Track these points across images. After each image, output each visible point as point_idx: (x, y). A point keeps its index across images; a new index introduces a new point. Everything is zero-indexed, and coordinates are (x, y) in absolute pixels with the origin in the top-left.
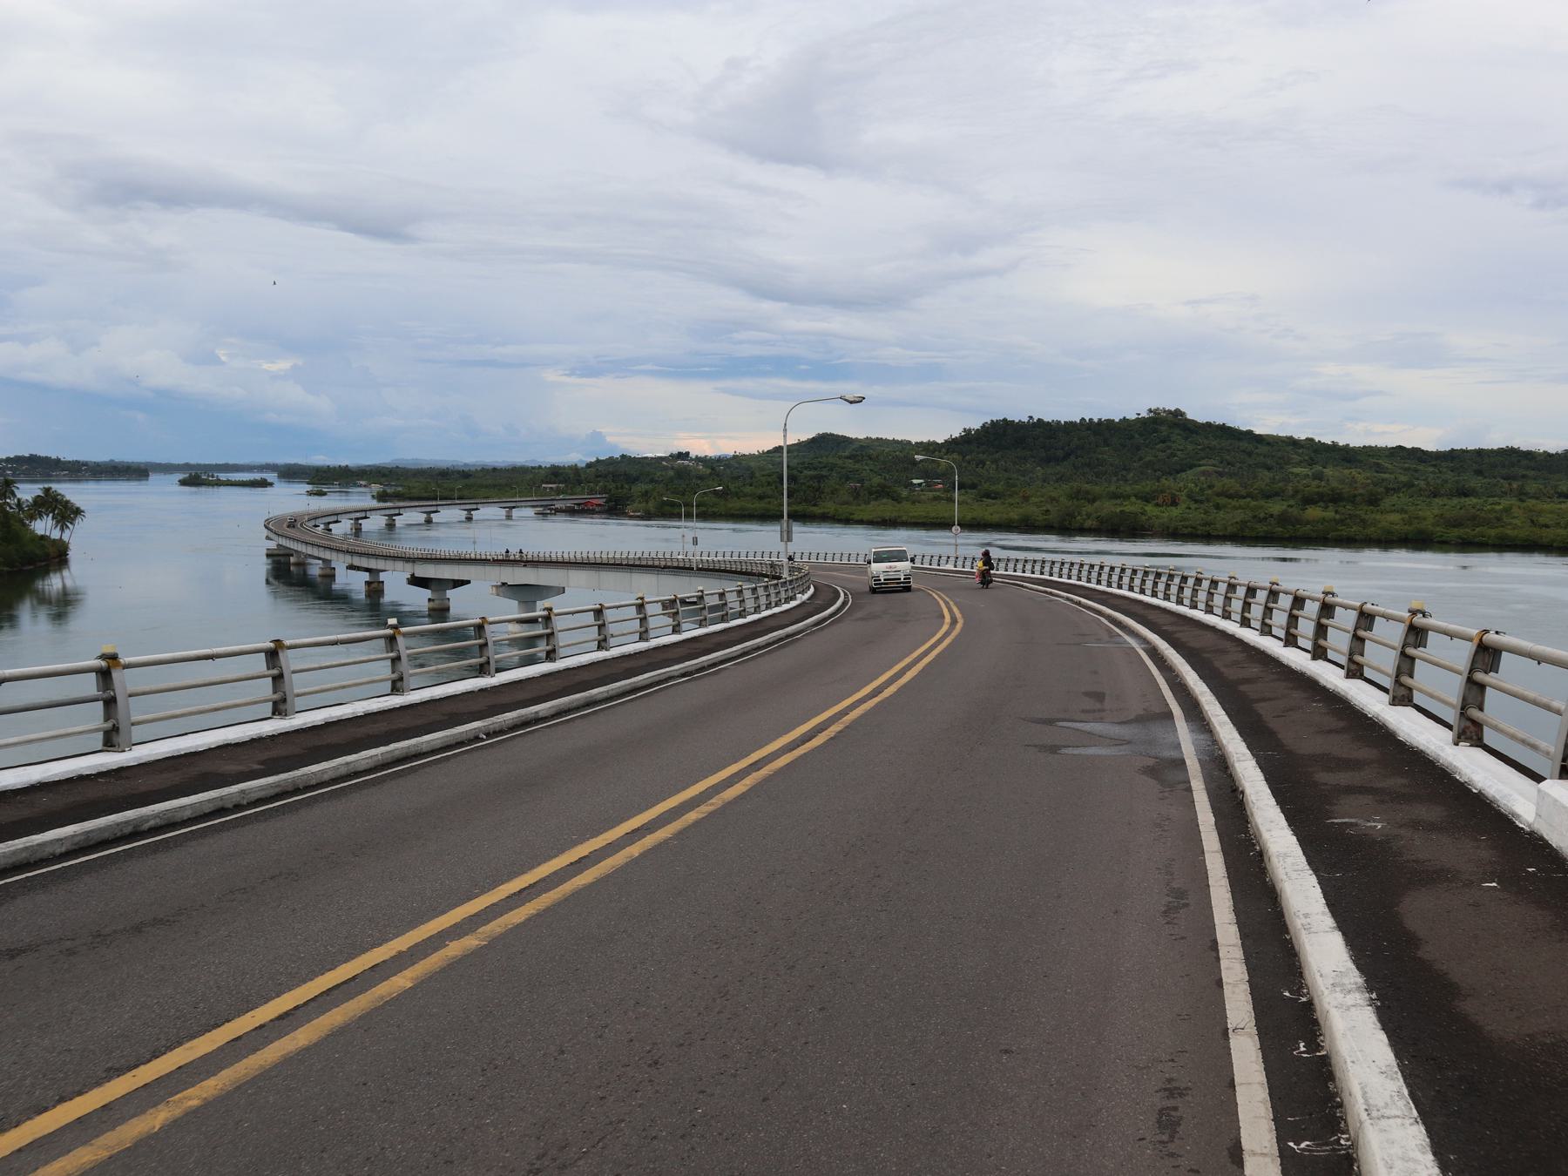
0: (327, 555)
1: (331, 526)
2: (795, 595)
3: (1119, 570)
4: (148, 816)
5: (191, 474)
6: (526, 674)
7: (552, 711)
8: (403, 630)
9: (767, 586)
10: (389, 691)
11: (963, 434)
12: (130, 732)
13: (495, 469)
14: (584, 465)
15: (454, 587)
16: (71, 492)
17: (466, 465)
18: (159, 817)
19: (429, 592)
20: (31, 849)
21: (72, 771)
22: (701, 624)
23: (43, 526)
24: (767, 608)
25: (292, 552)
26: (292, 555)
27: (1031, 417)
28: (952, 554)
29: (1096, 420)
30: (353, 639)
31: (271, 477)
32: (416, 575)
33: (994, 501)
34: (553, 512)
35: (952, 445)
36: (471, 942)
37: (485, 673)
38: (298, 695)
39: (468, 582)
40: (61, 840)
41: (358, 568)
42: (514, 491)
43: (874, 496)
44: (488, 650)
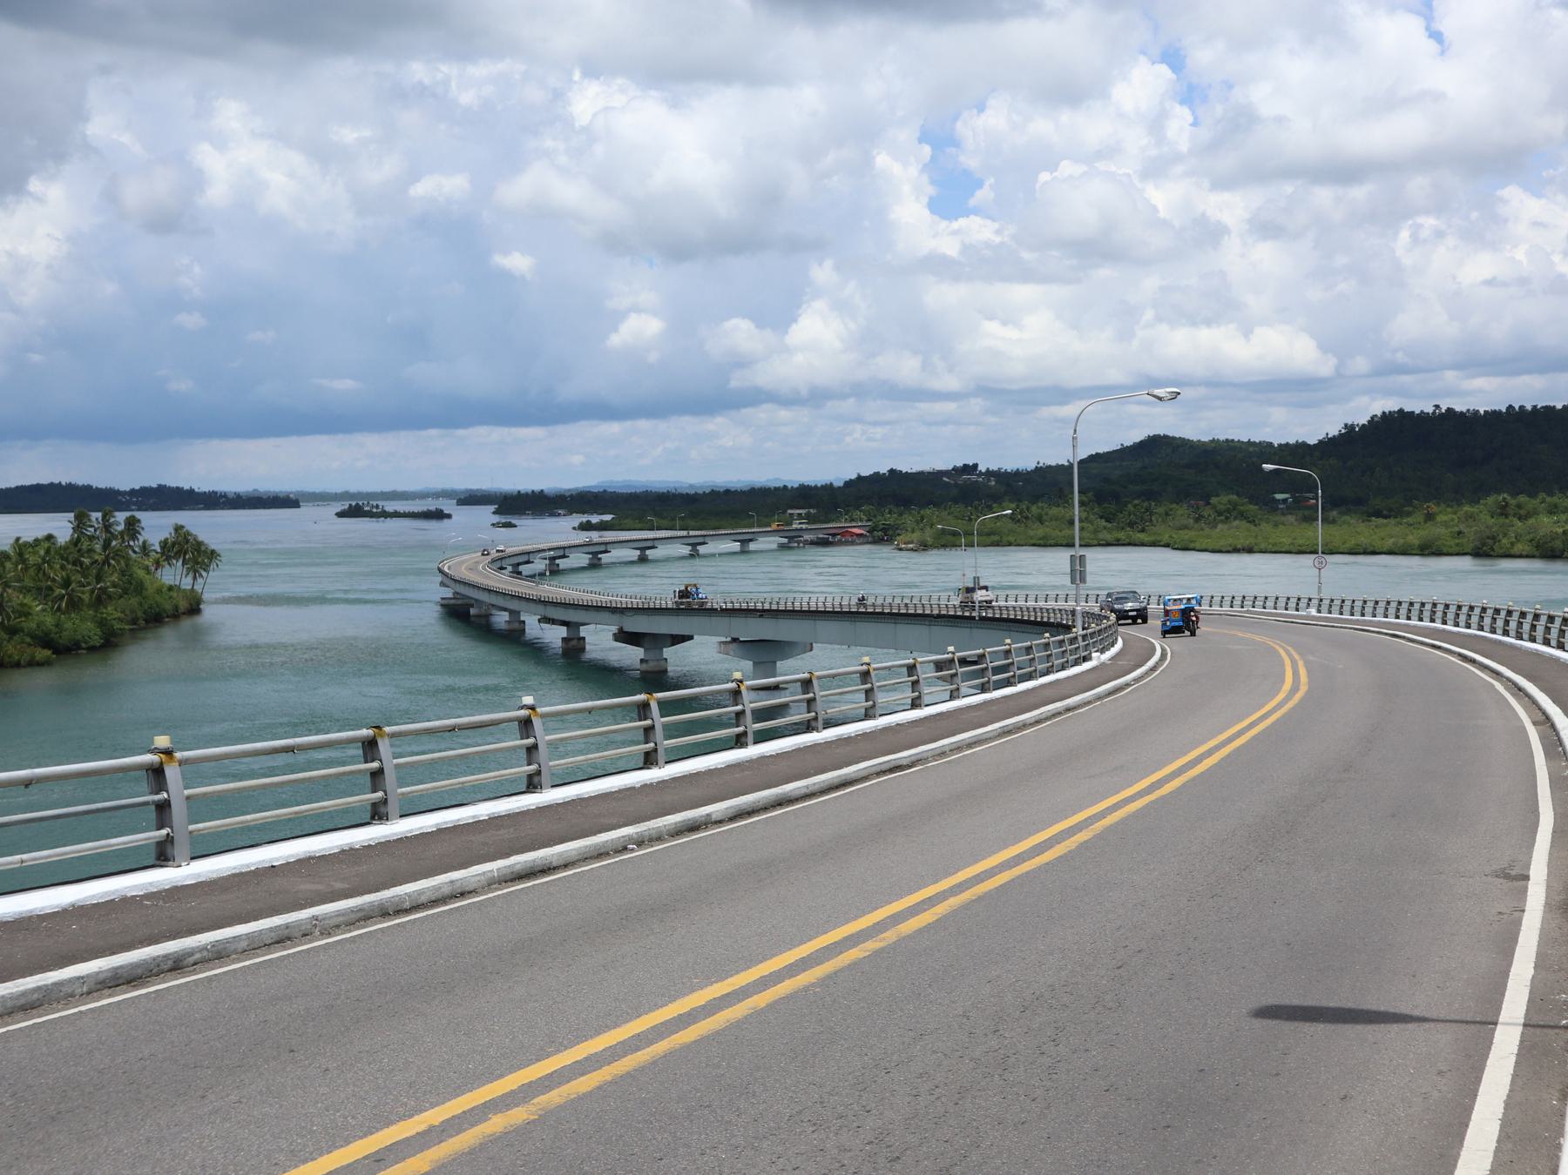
0: (514, 605)
1: (521, 568)
2: (1090, 654)
4: (192, 948)
5: (350, 505)
6: (706, 765)
7: (730, 813)
8: (387, 729)
9: (1031, 647)
11: (1343, 431)
13: (727, 492)
14: (841, 484)
15: (673, 645)
16: (203, 525)
17: (691, 486)
18: (208, 950)
19: (642, 650)
20: (45, 989)
21: (113, 892)
22: (983, 689)
23: (173, 575)
25: (473, 602)
26: (472, 606)
27: (1437, 407)
28: (1315, 595)
29: (1529, 408)
31: (447, 506)
32: (626, 629)
33: (1385, 521)
34: (801, 545)
35: (1328, 446)
36: (519, 1115)
37: (652, 764)
39: (690, 638)
40: (83, 978)
41: (553, 621)
42: (752, 520)
43: (1223, 518)
44: (654, 734)
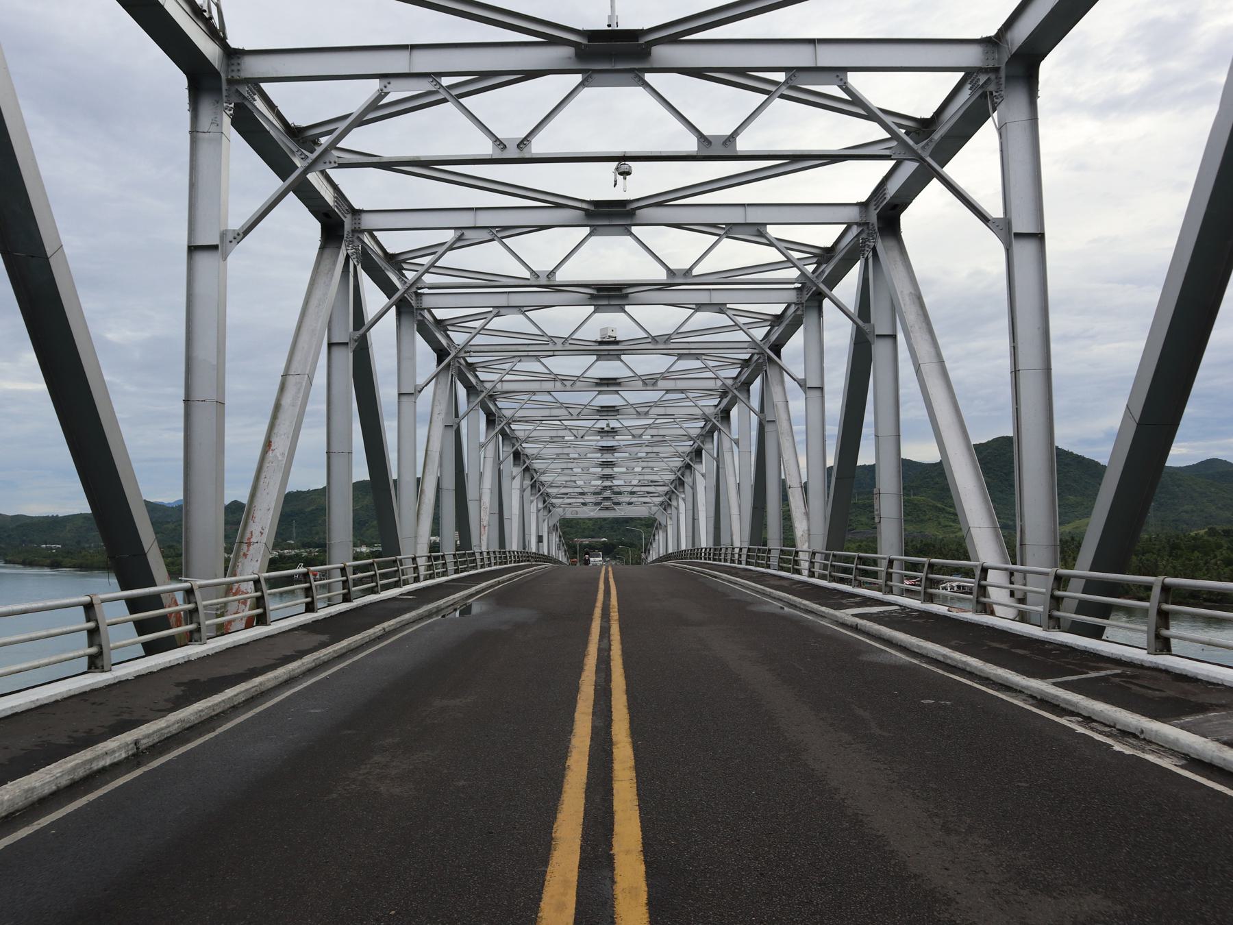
3: (746, 550)
10: (304, 611)
12: (110, 653)
24: (481, 568)
30: (117, 597)
38: (271, 611)
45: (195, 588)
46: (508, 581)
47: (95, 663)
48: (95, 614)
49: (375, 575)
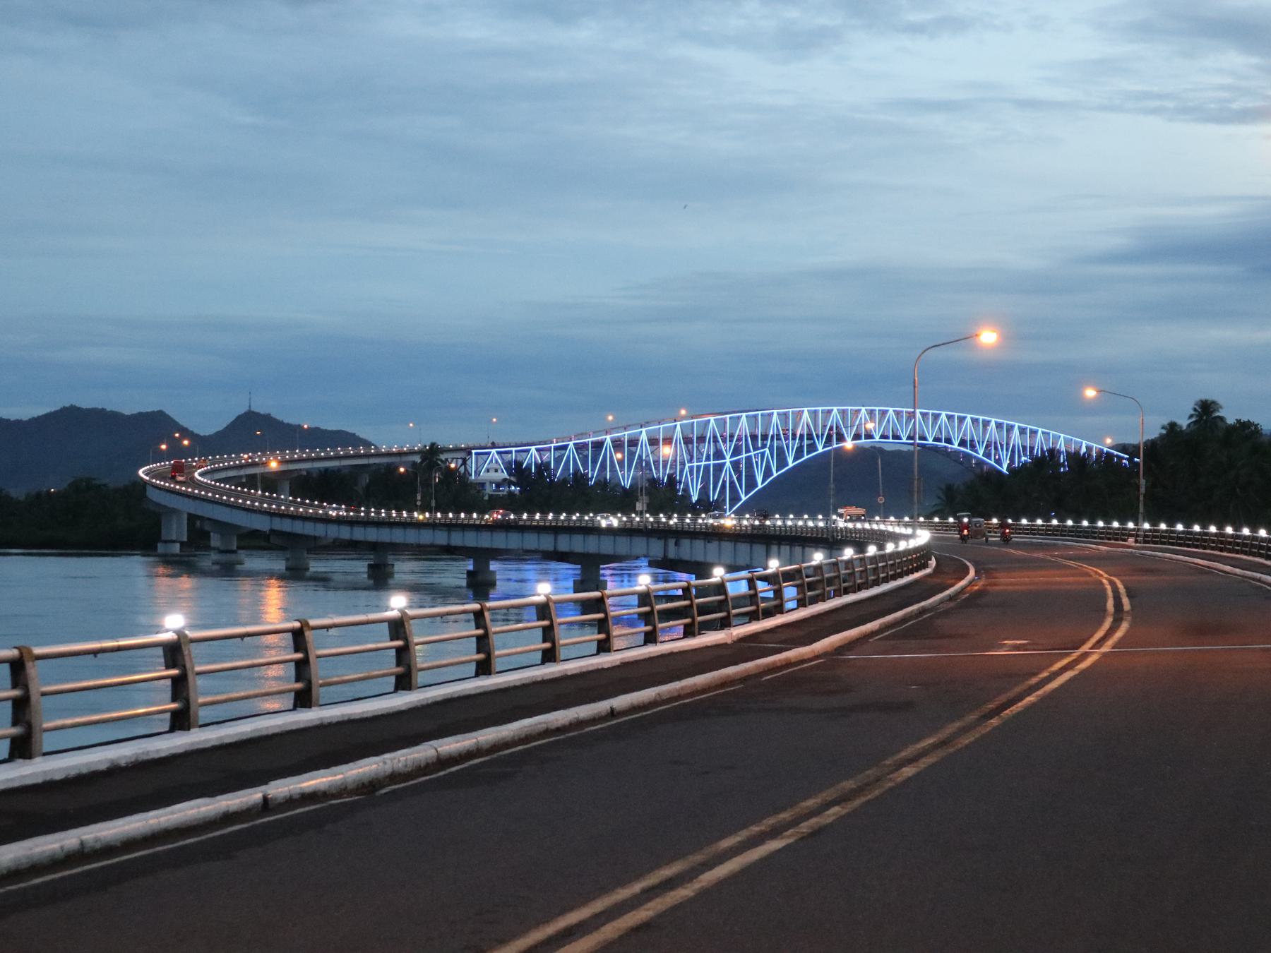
10: (473, 675)
45: (754, 578)
46: (1005, 585)
47: (549, 656)
48: (26, 678)
49: (691, 606)
